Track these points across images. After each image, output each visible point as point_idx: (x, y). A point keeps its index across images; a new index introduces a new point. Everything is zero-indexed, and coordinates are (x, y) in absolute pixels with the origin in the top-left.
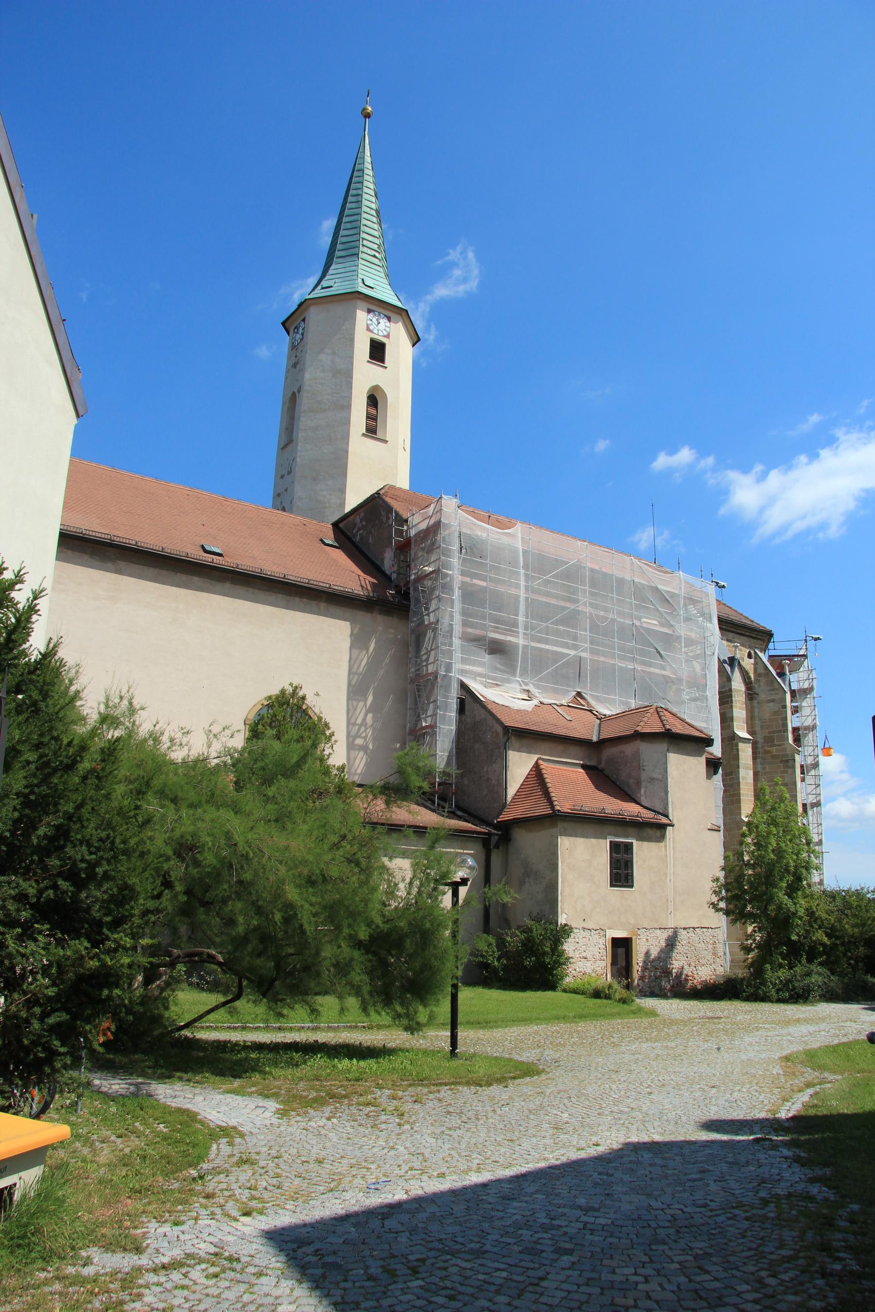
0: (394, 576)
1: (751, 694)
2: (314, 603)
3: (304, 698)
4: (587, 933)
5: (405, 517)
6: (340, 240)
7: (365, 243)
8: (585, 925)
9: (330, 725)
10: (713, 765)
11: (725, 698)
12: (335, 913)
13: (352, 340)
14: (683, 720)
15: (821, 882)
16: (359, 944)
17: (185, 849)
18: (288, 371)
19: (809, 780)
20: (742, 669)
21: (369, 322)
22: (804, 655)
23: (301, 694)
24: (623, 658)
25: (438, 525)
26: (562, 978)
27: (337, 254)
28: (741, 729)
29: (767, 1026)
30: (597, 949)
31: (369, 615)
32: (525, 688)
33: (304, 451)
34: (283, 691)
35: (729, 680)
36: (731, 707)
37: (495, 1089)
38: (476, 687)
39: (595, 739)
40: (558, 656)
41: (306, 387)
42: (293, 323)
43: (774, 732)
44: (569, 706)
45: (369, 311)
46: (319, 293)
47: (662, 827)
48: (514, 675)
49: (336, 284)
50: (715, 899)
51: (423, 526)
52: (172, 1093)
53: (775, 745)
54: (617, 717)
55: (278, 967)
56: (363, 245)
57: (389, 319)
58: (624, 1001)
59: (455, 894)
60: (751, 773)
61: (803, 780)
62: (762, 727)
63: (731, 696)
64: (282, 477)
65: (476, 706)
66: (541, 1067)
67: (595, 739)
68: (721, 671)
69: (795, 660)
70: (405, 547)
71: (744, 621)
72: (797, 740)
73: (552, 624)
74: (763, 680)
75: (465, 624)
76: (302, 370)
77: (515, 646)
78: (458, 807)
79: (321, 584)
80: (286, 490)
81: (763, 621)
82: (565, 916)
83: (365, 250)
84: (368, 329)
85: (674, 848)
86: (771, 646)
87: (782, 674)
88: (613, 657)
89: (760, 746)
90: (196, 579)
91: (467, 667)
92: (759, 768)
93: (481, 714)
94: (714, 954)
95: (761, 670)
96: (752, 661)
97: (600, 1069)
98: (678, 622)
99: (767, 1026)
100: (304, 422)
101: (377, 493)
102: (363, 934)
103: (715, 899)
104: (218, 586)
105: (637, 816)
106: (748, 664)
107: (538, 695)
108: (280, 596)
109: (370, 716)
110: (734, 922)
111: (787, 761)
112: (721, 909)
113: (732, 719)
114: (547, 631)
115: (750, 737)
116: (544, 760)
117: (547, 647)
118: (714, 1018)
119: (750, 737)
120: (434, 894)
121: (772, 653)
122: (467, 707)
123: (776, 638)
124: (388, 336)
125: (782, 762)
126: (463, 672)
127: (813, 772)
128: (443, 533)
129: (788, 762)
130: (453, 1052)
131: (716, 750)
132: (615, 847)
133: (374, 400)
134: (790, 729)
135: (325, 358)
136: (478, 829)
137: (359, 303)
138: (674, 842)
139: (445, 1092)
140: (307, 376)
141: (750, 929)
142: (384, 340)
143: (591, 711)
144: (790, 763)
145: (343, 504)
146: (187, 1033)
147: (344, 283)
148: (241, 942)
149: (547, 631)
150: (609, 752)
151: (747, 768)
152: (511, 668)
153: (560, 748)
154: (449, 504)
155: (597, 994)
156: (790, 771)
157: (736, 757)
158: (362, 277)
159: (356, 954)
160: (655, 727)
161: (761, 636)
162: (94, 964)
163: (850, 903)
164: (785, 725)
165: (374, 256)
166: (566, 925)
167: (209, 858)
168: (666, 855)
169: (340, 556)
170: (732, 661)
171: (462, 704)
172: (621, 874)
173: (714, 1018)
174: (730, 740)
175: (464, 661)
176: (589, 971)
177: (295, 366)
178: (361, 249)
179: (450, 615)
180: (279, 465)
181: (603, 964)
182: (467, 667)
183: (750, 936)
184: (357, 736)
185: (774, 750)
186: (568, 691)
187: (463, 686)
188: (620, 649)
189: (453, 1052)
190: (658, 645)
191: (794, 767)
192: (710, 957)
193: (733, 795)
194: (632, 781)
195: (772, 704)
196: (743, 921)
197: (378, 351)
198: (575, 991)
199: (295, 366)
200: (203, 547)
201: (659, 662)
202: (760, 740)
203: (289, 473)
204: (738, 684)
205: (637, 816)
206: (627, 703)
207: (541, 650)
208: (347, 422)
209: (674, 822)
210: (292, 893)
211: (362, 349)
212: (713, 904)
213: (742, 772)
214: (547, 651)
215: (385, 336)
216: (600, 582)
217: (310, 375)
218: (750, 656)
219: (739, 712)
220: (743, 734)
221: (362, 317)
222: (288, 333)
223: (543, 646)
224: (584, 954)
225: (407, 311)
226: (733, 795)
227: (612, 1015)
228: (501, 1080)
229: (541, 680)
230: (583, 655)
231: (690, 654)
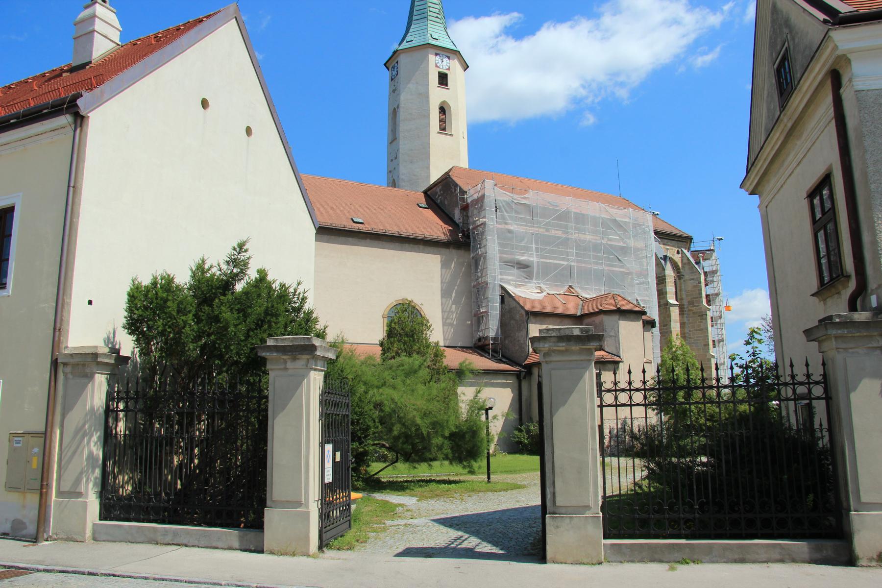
0: (461, 225)
1: (679, 275)
2: (416, 246)
5: (465, 189)
6: (416, 8)
7: (436, 15)
11: (661, 280)
12: (436, 425)
13: (427, 74)
16: (445, 438)
17: (378, 405)
24: (597, 264)
25: (483, 196)
27: (415, 18)
28: (672, 299)
33: (404, 145)
35: (664, 269)
37: (502, 493)
38: (510, 288)
40: (556, 266)
41: (402, 105)
42: (391, 63)
45: (437, 54)
46: (405, 45)
47: (617, 363)
48: (532, 279)
49: (415, 39)
51: (475, 196)
52: (379, 496)
54: (593, 299)
55: (413, 448)
57: (449, 58)
59: (487, 414)
60: (678, 324)
62: (687, 296)
65: (510, 299)
67: (579, 314)
68: (658, 264)
69: (706, 254)
70: (465, 208)
74: (687, 267)
75: (501, 252)
76: (399, 95)
77: (533, 262)
78: (503, 356)
81: (686, 231)
84: (437, 66)
86: (692, 245)
87: (698, 263)
90: (350, 239)
91: (505, 277)
92: (685, 320)
93: (513, 304)
95: (685, 261)
98: (629, 238)
100: (403, 127)
101: (447, 173)
102: (447, 434)
104: (363, 241)
106: (677, 258)
109: (454, 306)
120: (478, 415)
121: (692, 249)
123: (694, 240)
124: (448, 69)
126: (502, 280)
127: (719, 321)
128: (486, 200)
129: (703, 316)
130: (489, 481)
133: (443, 110)
135: (411, 86)
136: (514, 369)
137: (431, 50)
139: (481, 494)
140: (402, 98)
142: (446, 72)
145: (429, 177)
146: (376, 476)
148: (397, 438)
152: (529, 277)
153: (558, 320)
154: (489, 184)
157: (669, 316)
159: (446, 442)
161: (684, 240)
162: (361, 450)
164: (700, 294)
167: (387, 409)
169: (430, 214)
170: (665, 258)
171: (502, 298)
175: (501, 274)
177: (394, 91)
178: (429, 14)
179: (492, 248)
180: (389, 154)
182: (505, 277)
184: (447, 318)
187: (503, 288)
189: (489, 481)
190: (618, 254)
191: (706, 319)
197: (443, 79)
199: (394, 91)
201: (618, 263)
202: (685, 302)
204: (669, 272)
206: (600, 290)
208: (428, 125)
209: (624, 360)
210: (419, 421)
211: (434, 79)
213: (673, 325)
216: (580, 219)
217: (404, 97)
218: (678, 253)
219: (670, 289)
220: (673, 301)
221: (432, 59)
223: (548, 261)
228: (506, 490)
230: (572, 264)
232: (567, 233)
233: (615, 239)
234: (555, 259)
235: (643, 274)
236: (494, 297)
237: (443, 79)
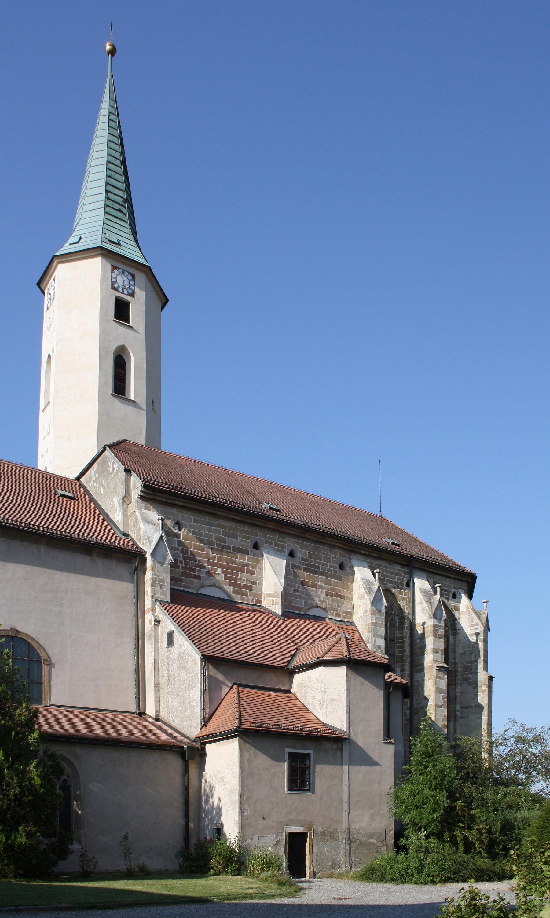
21: (114, 280)
142: (129, 298)
165: (120, 211)
215: (129, 295)
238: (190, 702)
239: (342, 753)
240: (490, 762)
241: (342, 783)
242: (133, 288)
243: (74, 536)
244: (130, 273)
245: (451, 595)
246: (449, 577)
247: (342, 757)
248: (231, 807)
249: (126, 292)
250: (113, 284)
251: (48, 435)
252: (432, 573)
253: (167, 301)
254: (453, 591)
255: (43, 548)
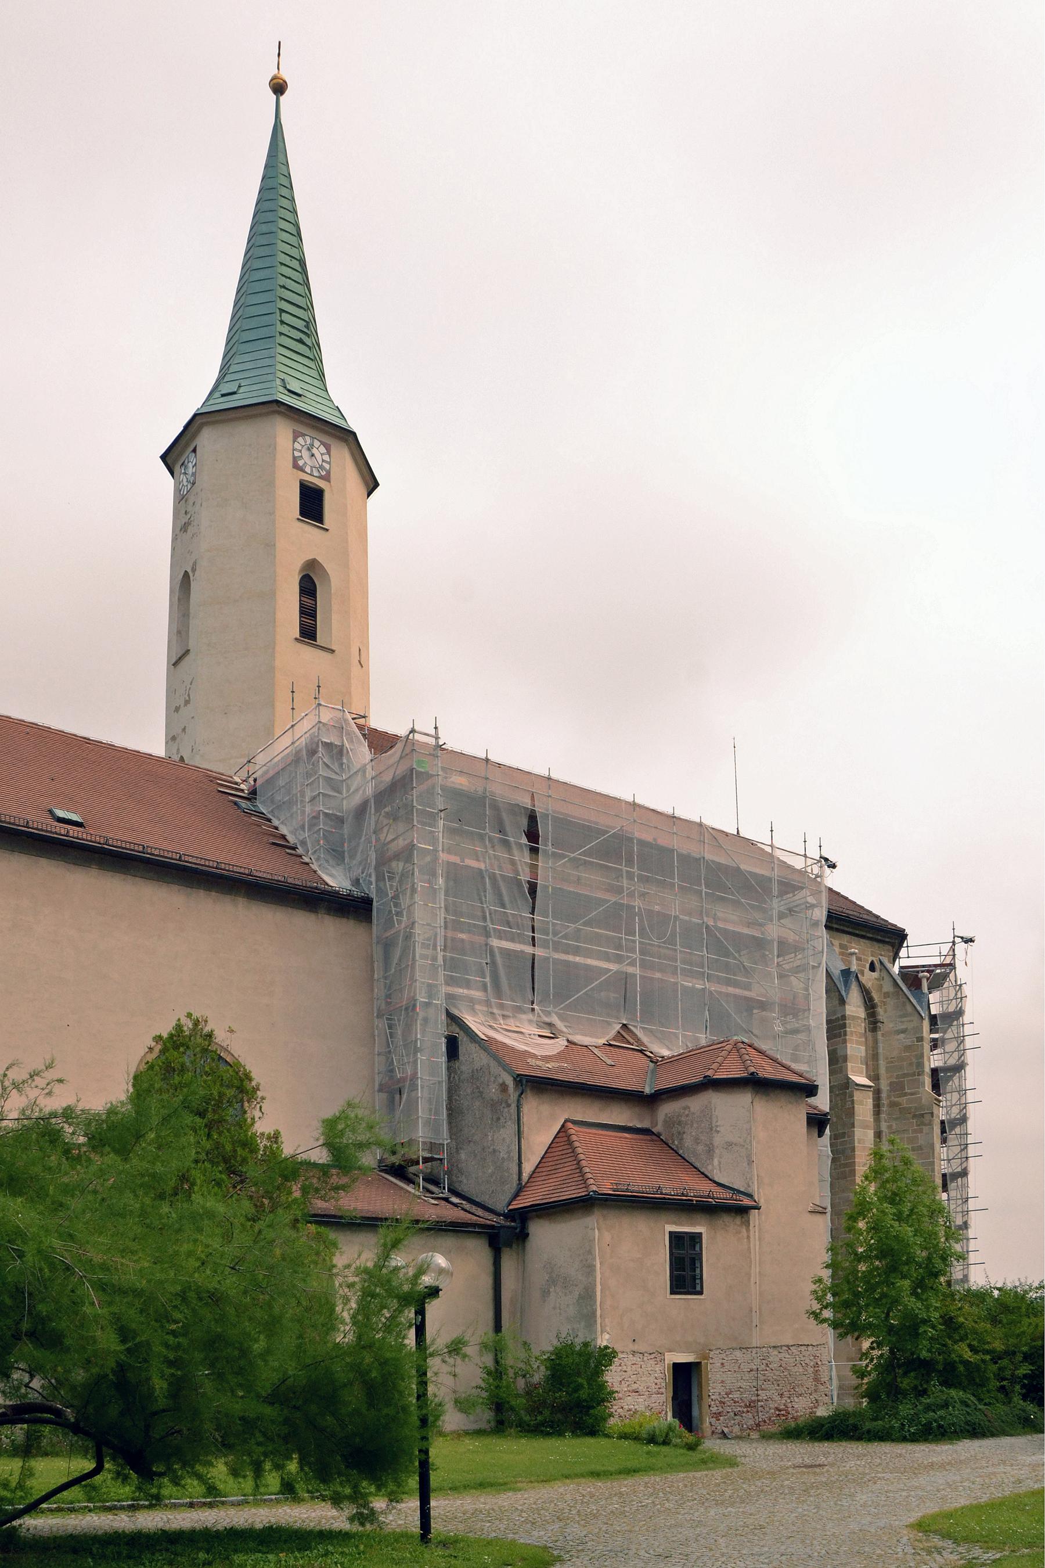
3: (210, 1036)
4: (637, 1359)
7: (286, 317)
8: (636, 1348)
9: (253, 1075)
10: (817, 1122)
11: (836, 1028)
14: (775, 1060)
15: (965, 1279)
18: (175, 539)
19: (952, 1138)
20: (861, 986)
21: (297, 454)
22: (950, 964)
23: (207, 1029)
24: (688, 973)
26: (605, 1420)
28: (859, 1073)
29: (887, 1476)
30: (652, 1379)
31: (312, 917)
32: (547, 1020)
34: (179, 1027)
35: (842, 1002)
36: (845, 1042)
39: (647, 1090)
43: (905, 1075)
44: (610, 1045)
50: (816, 1307)
53: (906, 1094)
56: (282, 322)
58: (692, 1447)
60: (871, 1133)
61: (944, 1141)
63: (844, 1026)
64: (177, 709)
66: (555, 1553)
68: (832, 989)
71: (865, 916)
72: (936, 1086)
73: (585, 924)
79: (236, 869)
80: (184, 730)
82: (607, 1336)
83: (285, 329)
84: (296, 466)
85: (760, 1239)
86: (903, 952)
88: (675, 973)
89: (884, 1095)
94: (816, 1380)
96: (875, 975)
97: (642, 1553)
99: (887, 1476)
103: (816, 1307)
105: (709, 1197)
107: (565, 1030)
108: (175, 887)
110: (841, 1336)
111: (922, 1115)
112: (824, 1321)
113: (845, 1059)
114: (577, 935)
115: (871, 1084)
116: (574, 1122)
117: (578, 959)
118: (816, 1466)
119: (871, 1084)
122: (462, 1050)
123: (910, 940)
125: (914, 1116)
129: (922, 1116)
131: (822, 1101)
132: (676, 1239)
133: (308, 587)
134: (927, 1070)
138: (760, 1230)
141: (866, 1344)
142: (321, 484)
143: (641, 1051)
144: (927, 1117)
147: (255, 387)
149: (577, 935)
150: (667, 1109)
151: (866, 1127)
155: (652, 1439)
156: (925, 1129)
157: (851, 1112)
158: (283, 376)
160: (733, 1070)
163: (1011, 1307)
164: (920, 1065)
165: (301, 341)
166: (606, 1347)
168: (749, 1248)
172: (685, 1275)
173: (816, 1466)
174: (842, 1088)
176: (641, 1408)
180: (171, 692)
181: (663, 1398)
183: (864, 1355)
185: (903, 1101)
186: (609, 1023)
187: (452, 1018)
188: (683, 962)
192: (810, 1383)
193: (846, 1165)
194: (700, 1148)
195: (902, 1035)
196: (856, 1334)
197: (312, 504)
198: (624, 1436)
200: (51, 812)
203: (187, 702)
205: (709, 1197)
206: (697, 1039)
207: (567, 963)
209: (762, 1203)
212: (813, 1313)
214: (576, 965)
215: (321, 477)
218: (872, 968)
222: (172, 473)
223: (570, 958)
224: (635, 1387)
225: (354, 434)
226: (846, 1165)
227: (671, 1468)
229: (568, 1008)
230: (630, 970)
231: (786, 967)
232: (619, 890)
233: (729, 919)
234: (589, 954)
235: (793, 1009)
236: (431, 1038)
237: (312, 504)
238: (494, 1151)
239: (748, 1230)
240: (175, 1471)
241: (749, 1279)
242: (327, 466)
243: (255, 873)
244: (322, 443)
245: (868, 966)
246: (863, 937)
247: (748, 1237)
248: (583, 1324)
249: (316, 474)
250: (295, 459)
251: (186, 705)
252: (837, 930)
253: (376, 485)
254: (870, 959)
255: (241, 902)
